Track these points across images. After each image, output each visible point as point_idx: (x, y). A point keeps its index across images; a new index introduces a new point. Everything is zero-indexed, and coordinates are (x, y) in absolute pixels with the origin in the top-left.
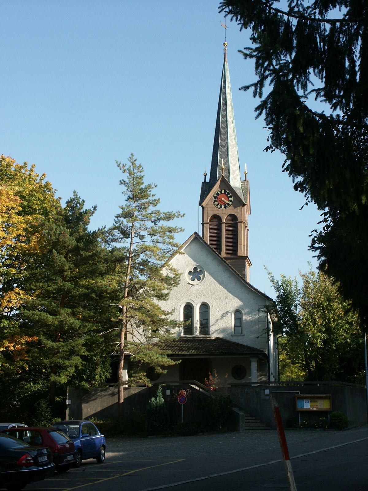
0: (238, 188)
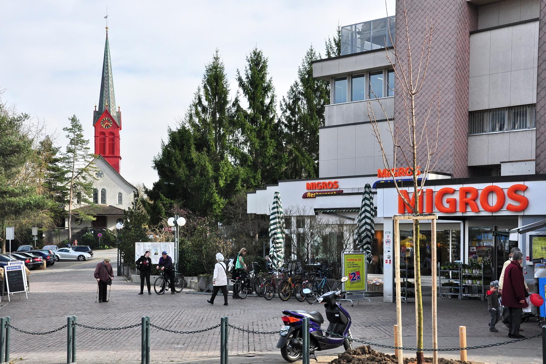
0: (115, 117)
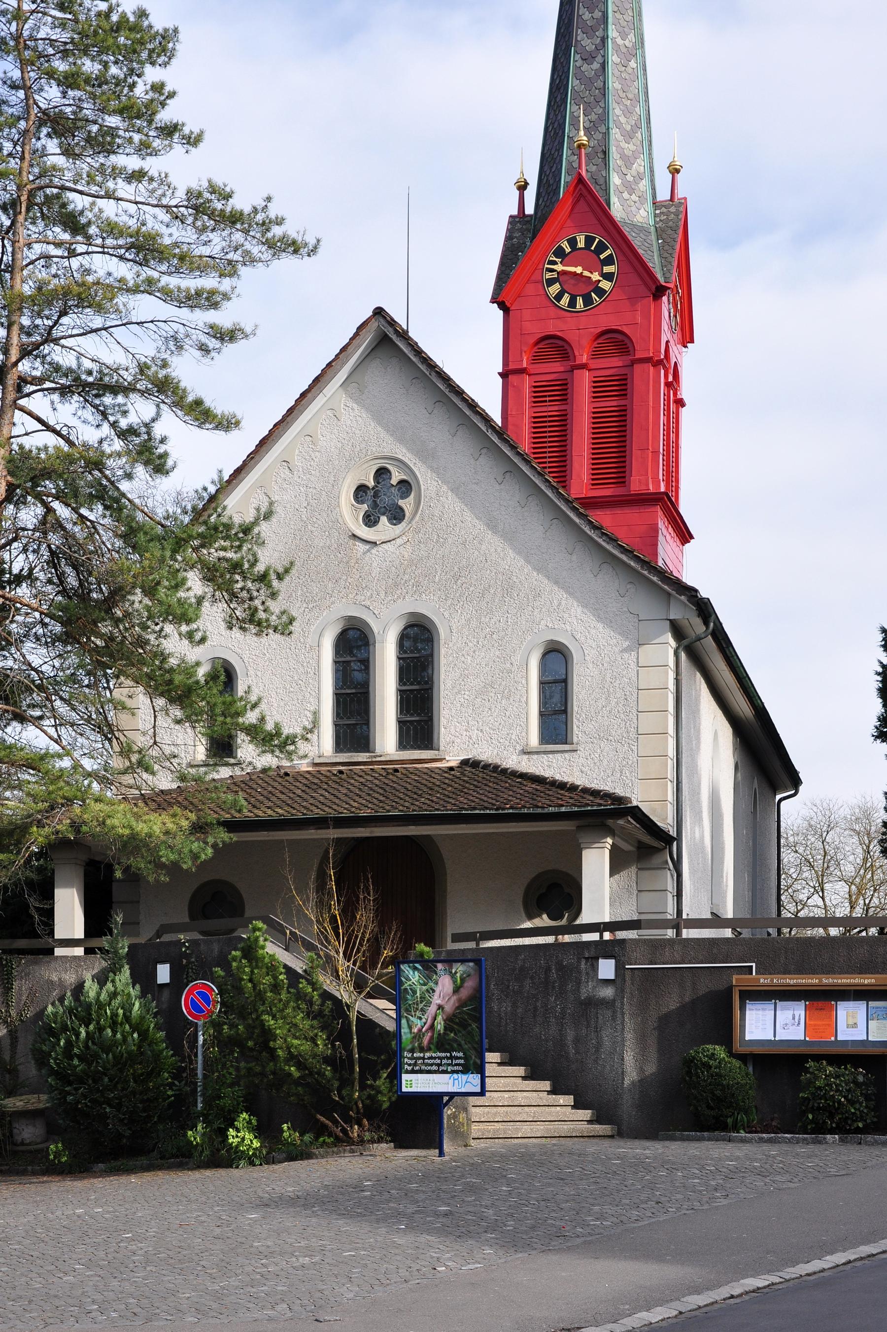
0: (642, 229)
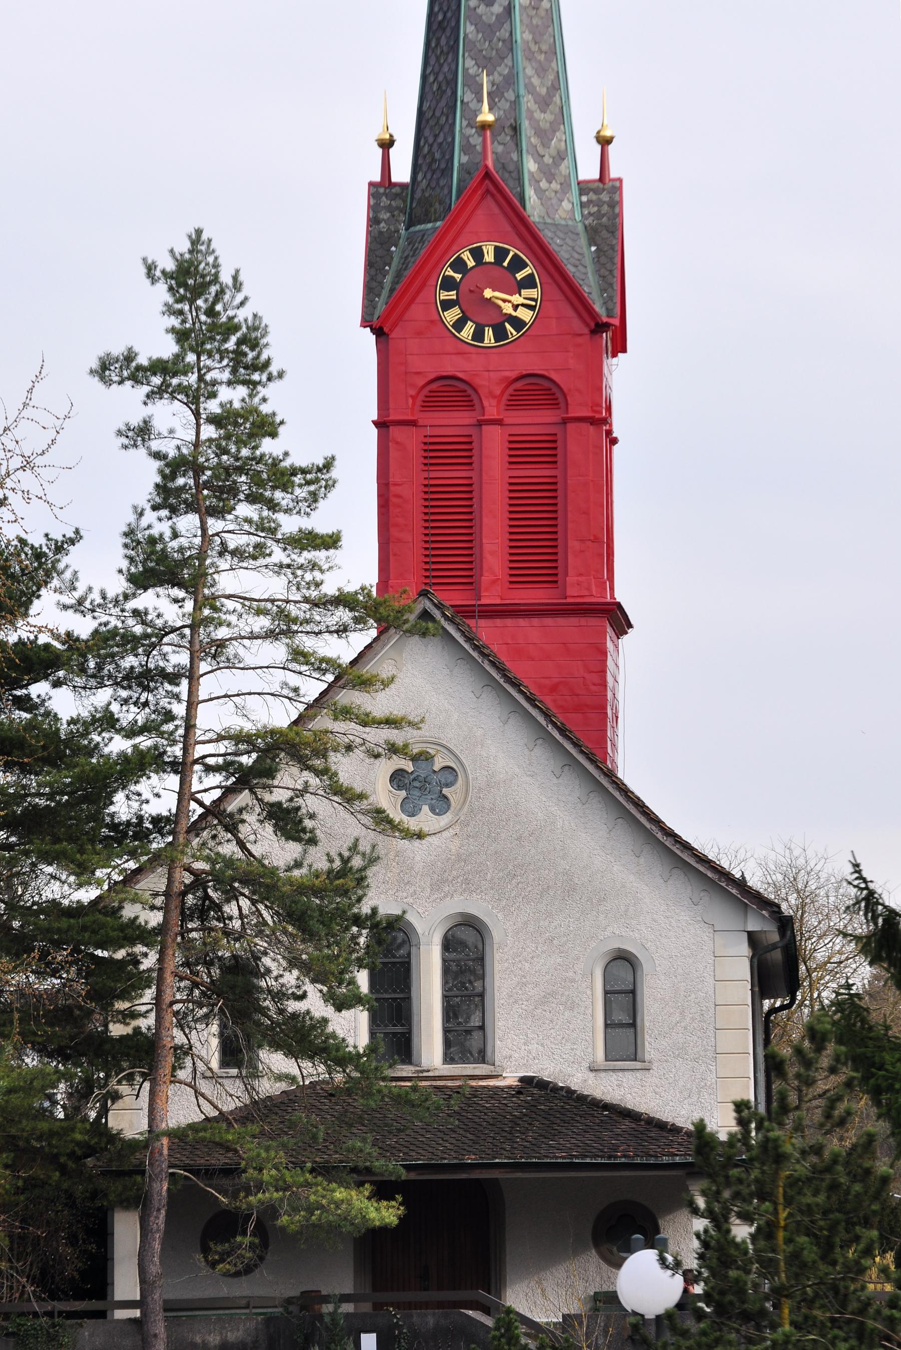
0: (568, 231)
